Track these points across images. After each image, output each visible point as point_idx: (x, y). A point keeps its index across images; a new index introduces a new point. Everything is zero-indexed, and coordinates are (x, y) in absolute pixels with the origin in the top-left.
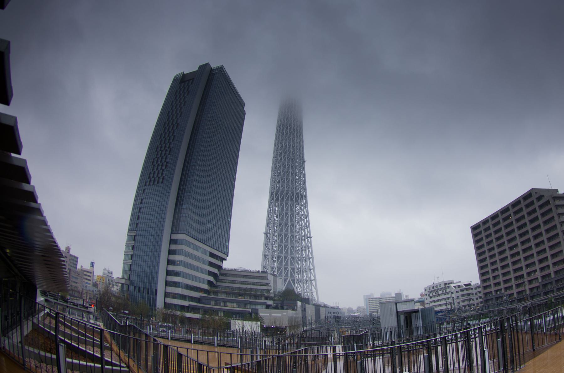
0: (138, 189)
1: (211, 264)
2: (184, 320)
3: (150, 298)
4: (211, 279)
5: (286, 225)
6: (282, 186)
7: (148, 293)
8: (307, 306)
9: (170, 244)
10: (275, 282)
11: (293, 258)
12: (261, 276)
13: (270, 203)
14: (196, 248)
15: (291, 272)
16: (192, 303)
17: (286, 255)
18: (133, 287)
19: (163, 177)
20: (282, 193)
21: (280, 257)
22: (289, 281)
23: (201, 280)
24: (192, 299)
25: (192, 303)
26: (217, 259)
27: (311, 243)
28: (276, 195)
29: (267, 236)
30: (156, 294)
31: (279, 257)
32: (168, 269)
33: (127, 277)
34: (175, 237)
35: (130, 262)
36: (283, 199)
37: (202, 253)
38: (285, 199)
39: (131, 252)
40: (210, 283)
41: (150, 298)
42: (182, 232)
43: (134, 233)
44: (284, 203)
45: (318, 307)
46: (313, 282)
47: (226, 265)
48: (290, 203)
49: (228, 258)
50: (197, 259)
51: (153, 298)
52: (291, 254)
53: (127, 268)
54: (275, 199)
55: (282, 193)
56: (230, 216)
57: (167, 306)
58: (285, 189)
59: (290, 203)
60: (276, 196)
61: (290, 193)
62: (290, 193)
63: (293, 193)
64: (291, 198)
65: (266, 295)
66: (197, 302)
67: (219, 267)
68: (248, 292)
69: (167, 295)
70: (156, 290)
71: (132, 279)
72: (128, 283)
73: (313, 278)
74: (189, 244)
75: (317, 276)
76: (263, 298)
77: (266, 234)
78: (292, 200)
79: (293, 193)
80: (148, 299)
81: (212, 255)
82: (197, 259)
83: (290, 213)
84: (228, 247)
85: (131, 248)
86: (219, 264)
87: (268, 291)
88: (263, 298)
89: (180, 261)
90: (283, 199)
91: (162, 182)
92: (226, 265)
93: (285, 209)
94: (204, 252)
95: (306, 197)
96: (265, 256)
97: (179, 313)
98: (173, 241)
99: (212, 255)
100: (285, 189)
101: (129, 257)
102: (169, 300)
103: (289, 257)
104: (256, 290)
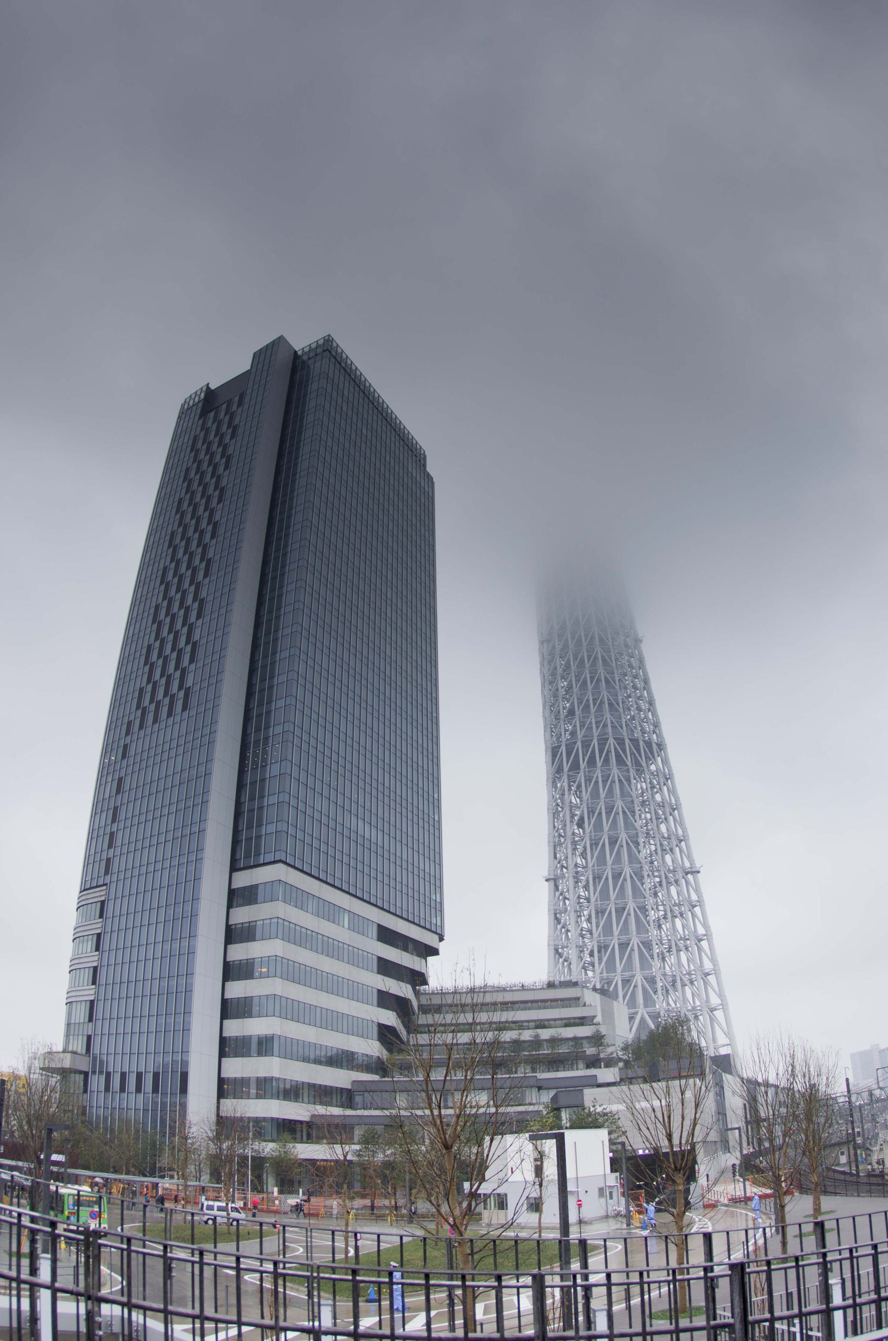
0: (107, 750)
1: (385, 967)
2: (289, 1175)
3: (164, 1104)
4: (390, 1018)
5: (613, 841)
6: (582, 726)
7: (155, 1089)
8: (727, 1077)
9: (230, 906)
10: (609, 1015)
11: (647, 945)
12: (560, 992)
13: (553, 782)
14: (331, 913)
15: (645, 990)
16: (321, 1110)
17: (624, 938)
18: (103, 1078)
19: (188, 691)
20: (586, 744)
21: (606, 947)
22: (643, 1020)
23: (353, 1027)
24: (322, 1094)
25: (321, 1110)
26: (405, 949)
27: (697, 891)
28: (569, 754)
29: (556, 888)
30: (184, 1089)
31: (602, 948)
32: (228, 996)
33: (79, 1045)
34: (243, 879)
35: (89, 992)
36: (592, 762)
37: (352, 928)
38: (599, 763)
39: (93, 959)
40: (386, 1034)
41: (164, 1104)
42: (270, 858)
43: (99, 894)
44: (598, 773)
45: (752, 1086)
46: (719, 1014)
47: (443, 974)
48: (615, 771)
49: (442, 947)
50: (331, 948)
51: (173, 1104)
52: (639, 931)
53: (81, 1013)
54: (566, 768)
55: (586, 744)
56: (436, 804)
57: (225, 1126)
58: (596, 733)
59: (615, 771)
60: (570, 759)
61: (611, 741)
62: (611, 741)
63: (620, 742)
64: (618, 756)
65: (590, 1051)
66: (342, 1106)
67: (417, 978)
68: (522, 1061)
69: (225, 1088)
70: (184, 1076)
71: (96, 1049)
72: (84, 1064)
73: (715, 1000)
74: (297, 897)
75: (728, 994)
76: (581, 1065)
77: (554, 881)
78: (620, 761)
79: (620, 742)
80: (154, 1110)
81: (386, 935)
82: (331, 948)
83: (619, 804)
84: (438, 908)
85: (90, 945)
86: (417, 968)
87: (597, 1039)
88: (581, 1065)
89: (274, 960)
90: (592, 762)
91: (184, 708)
92: (443, 974)
93: (603, 795)
94: (358, 924)
95: (661, 746)
96: (556, 950)
97: (269, 1148)
98: (237, 897)
99: (386, 935)
100: (596, 733)
101: (87, 975)
102: (234, 1107)
103: (635, 941)
104: (554, 1042)
